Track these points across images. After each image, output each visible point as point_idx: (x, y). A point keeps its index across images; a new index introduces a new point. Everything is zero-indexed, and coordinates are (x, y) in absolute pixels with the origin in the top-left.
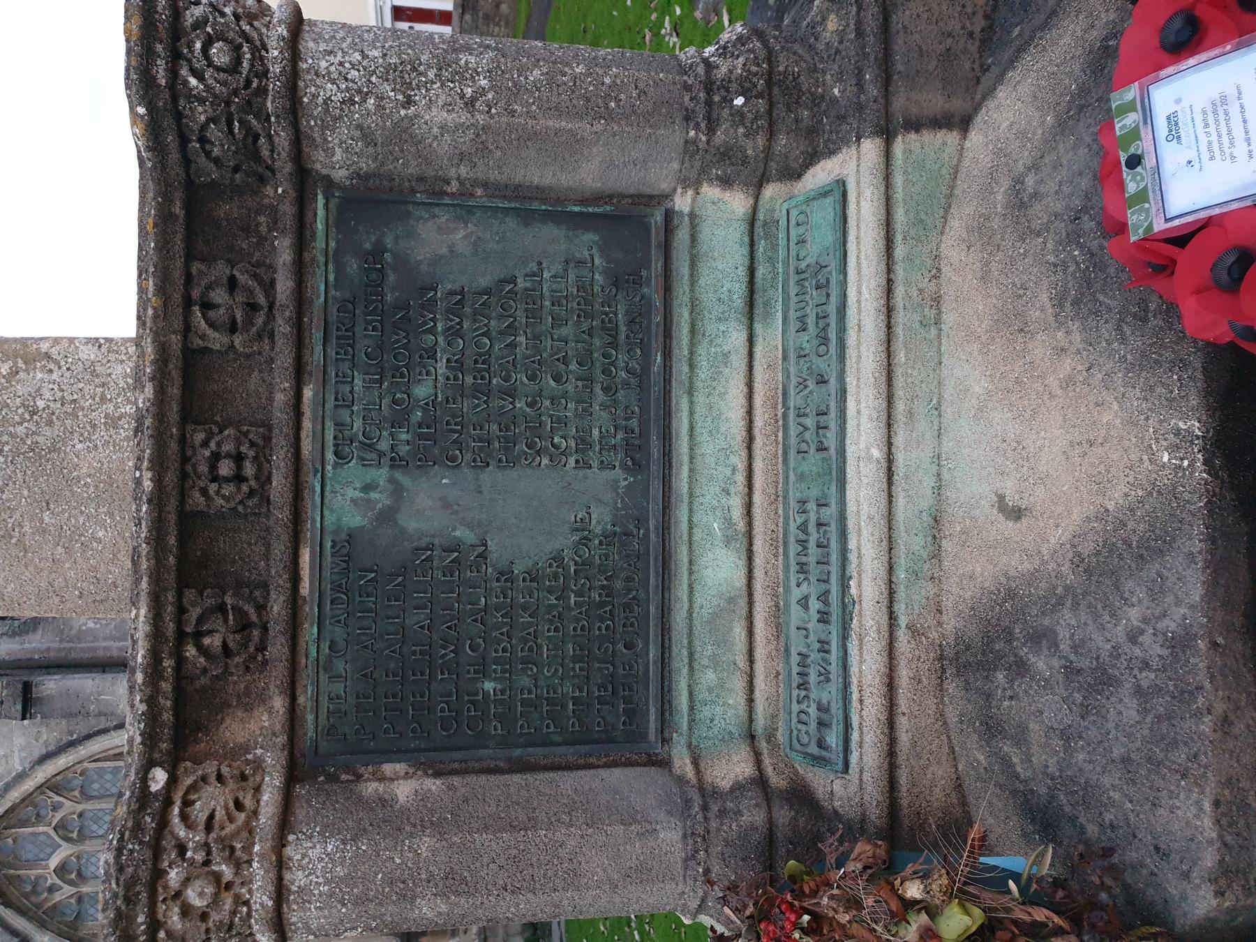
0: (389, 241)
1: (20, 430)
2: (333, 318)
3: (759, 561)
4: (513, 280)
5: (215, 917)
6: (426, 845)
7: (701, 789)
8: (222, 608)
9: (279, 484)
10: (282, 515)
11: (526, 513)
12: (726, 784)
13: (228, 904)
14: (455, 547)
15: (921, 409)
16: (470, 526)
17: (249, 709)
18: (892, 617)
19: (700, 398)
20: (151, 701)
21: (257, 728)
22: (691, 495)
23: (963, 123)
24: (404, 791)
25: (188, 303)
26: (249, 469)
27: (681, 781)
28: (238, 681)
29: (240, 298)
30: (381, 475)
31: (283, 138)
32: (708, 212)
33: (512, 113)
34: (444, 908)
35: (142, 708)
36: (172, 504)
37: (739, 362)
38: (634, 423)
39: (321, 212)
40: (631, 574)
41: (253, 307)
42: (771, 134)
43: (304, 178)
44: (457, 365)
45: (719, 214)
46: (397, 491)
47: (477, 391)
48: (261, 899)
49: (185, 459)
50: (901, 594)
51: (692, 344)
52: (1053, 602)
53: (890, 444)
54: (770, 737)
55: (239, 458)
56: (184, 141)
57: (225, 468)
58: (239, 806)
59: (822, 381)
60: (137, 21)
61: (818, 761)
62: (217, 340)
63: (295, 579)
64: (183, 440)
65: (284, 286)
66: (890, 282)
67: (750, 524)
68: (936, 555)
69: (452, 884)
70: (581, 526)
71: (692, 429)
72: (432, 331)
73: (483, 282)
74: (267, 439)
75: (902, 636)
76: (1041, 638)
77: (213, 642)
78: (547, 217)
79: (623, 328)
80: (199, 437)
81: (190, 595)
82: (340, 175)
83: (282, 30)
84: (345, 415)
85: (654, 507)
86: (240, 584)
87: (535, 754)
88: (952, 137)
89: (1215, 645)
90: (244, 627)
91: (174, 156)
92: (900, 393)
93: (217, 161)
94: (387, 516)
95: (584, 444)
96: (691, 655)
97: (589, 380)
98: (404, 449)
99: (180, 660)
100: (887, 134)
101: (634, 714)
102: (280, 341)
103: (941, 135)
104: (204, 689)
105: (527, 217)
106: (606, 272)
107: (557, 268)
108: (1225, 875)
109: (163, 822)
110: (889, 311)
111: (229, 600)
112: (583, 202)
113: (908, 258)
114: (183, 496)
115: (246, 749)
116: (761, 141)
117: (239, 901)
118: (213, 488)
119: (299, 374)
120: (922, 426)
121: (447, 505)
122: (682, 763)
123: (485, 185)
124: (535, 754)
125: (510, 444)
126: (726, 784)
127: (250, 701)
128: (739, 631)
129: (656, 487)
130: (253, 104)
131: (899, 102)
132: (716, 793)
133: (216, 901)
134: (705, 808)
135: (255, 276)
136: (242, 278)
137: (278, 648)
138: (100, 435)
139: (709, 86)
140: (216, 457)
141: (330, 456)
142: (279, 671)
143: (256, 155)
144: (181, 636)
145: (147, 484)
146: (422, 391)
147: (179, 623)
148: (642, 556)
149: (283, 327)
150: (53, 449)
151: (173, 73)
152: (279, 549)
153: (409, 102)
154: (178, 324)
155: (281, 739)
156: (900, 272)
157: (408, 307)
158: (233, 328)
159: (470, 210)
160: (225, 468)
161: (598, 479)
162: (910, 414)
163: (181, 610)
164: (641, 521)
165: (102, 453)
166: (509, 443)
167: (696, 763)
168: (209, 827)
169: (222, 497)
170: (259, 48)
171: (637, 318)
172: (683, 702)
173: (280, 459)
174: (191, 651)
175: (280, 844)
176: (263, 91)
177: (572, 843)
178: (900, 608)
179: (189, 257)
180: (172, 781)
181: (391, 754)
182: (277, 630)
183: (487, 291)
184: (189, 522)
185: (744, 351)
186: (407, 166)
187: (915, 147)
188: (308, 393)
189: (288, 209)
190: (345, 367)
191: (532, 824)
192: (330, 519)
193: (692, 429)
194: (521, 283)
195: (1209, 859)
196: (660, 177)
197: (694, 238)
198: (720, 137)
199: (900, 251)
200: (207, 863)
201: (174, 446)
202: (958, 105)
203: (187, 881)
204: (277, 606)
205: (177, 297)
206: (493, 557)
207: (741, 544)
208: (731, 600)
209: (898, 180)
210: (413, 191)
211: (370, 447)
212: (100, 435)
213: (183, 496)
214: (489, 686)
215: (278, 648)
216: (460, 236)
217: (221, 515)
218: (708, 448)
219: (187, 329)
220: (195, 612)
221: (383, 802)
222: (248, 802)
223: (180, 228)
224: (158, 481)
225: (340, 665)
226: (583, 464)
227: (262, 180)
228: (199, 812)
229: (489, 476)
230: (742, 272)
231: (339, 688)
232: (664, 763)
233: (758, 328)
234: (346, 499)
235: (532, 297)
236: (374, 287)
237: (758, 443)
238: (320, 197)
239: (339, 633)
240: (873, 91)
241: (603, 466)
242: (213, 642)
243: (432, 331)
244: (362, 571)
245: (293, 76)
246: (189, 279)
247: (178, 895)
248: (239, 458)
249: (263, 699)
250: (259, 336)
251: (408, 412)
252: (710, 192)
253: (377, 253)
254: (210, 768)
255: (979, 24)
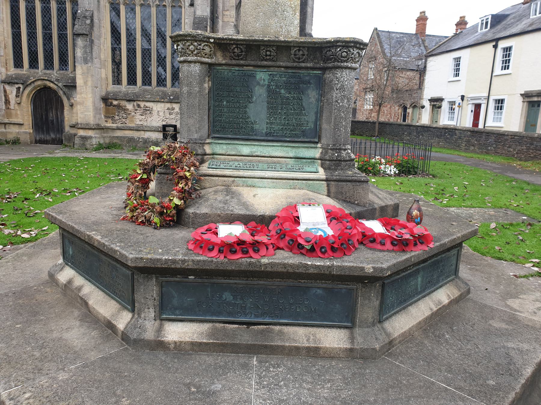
0: (312, 85)
1: (280, 9)
2: (297, 74)
3: (247, 158)
4: (304, 110)
5: (188, 50)
6: (197, 89)
7: (204, 143)
8: (242, 52)
9: (265, 63)
10: (259, 63)
11: (258, 112)
12: (205, 148)
13: (189, 53)
14: (252, 97)
15: (275, 184)
16: (256, 100)
17: (223, 56)
18: (236, 177)
19: (280, 148)
20: (226, 39)
21: (219, 58)
22: (261, 145)
23: (328, 196)
24: (206, 85)
25: (299, 47)
26: (268, 57)
27: (205, 140)
28: (228, 54)
29: (301, 57)
30: (266, 83)
31: (330, 65)
32: (317, 150)
33: (335, 110)
34: (185, 92)
35: (225, 37)
36: (261, 43)
37: (286, 155)
38: (275, 134)
39: (318, 72)
40: (247, 134)
41: (299, 59)
42: (329, 160)
43: (324, 69)
44: (288, 98)
45: (316, 153)
46: (263, 86)
47: (282, 102)
48: (190, 58)
49: (270, 46)
50: (240, 179)
51: (291, 147)
52: (239, 200)
53: (268, 179)
54: (213, 158)
55: (270, 55)
56: (329, 47)
57: (268, 53)
58: (206, 55)
59: (281, 168)
60: (348, 40)
61: (210, 164)
62: (293, 52)
63: (247, 66)
64: (273, 46)
65: (303, 65)
66: (298, 180)
67: (254, 156)
68: (247, 186)
69: (189, 93)
70: (255, 122)
71: (274, 146)
72: (294, 93)
73: (304, 104)
74: (274, 61)
75: (233, 179)
76: (232, 198)
77: (236, 50)
78: (316, 117)
79: (294, 132)
80: (274, 49)
81: (245, 46)
82: (325, 76)
83: (350, 66)
84: (278, 76)
85: (258, 138)
86: (246, 55)
87: (211, 111)
88: (326, 193)
89: (232, 214)
90: (238, 56)
91: (326, 45)
92: (277, 181)
93: (326, 53)
94: (258, 84)
95: (272, 123)
96: (229, 144)
97: (284, 125)
98: (271, 87)
99: (233, 44)
100: (327, 180)
101: (218, 132)
102: (292, 64)
103: (326, 191)
104: (227, 48)
105: (316, 113)
106: (305, 129)
107: (306, 119)
108: (195, 214)
109: (204, 42)
110: (293, 179)
111: (243, 53)
112: (320, 125)
113: (303, 183)
114: (263, 45)
115: (215, 56)
116: (328, 158)
117: (189, 55)
118: (265, 51)
119: (286, 67)
120: (271, 185)
121: (260, 95)
122: (208, 141)
123: (323, 105)
124: (211, 111)
125: (272, 108)
126: (205, 148)
127: (224, 57)
128: (233, 153)
129: (262, 138)
130: (336, 60)
131: (333, 183)
132: (203, 146)
133: (190, 50)
134: (201, 143)
135: (305, 59)
136: (304, 57)
137: (234, 62)
138: (278, 24)
139: (340, 149)
140: (270, 51)
141: (270, 73)
142: (230, 62)
143: (328, 60)
144: (237, 44)
145: (265, 39)
146: (283, 91)
147: (239, 44)
148: (249, 135)
149: (295, 64)
150: (276, 15)
151: (340, 46)
152: (253, 63)
153: (337, 89)
154: (295, 45)
155: (217, 62)
156: (300, 181)
157: (299, 89)
158: (295, 55)
159: (318, 102)
160: (268, 53)
161: (265, 126)
162: (274, 182)
163: (242, 45)
164: (256, 135)
165: (274, 25)
166: (272, 108)
167: (208, 143)
168: (203, 49)
169: (263, 52)
170: (345, 61)
171: (296, 136)
172: (216, 142)
173: (270, 63)
174: (234, 46)
175: (199, 62)
176: (338, 62)
177: (196, 117)
178: (238, 179)
179: (308, 47)
180: (211, 43)
181: (213, 83)
182: (238, 62)
183: (302, 105)
184: (258, 47)
185: (289, 156)
186: (326, 89)
187: (324, 186)
188: (283, 69)
189: (318, 66)
190: (287, 76)
191: (200, 109)
192: (258, 73)
193: (274, 146)
194: (303, 112)
195: (198, 212)
196: (324, 141)
197: (312, 147)
198: (330, 151)
199: (304, 182)
200: (197, 49)
201: (272, 44)
202: (332, 195)
203: (194, 46)
204: (242, 62)
205: (300, 45)
206: (249, 104)
207: (251, 154)
208: (240, 152)
209: (318, 182)
210: (322, 90)
211: (272, 80)
212: (278, 24)
213: (263, 45)
214: (225, 103)
215: (234, 62)
216: (313, 100)
217: (260, 52)
218: (270, 149)
219: (295, 47)
220: (241, 47)
221: (205, 81)
222: (206, 56)
223: (313, 46)
224: (266, 41)
225: (230, 74)
226: (267, 123)
227: (324, 61)
228: (206, 48)
229: (266, 104)
230: (304, 156)
231: (226, 73)
232: (208, 138)
233: (293, 159)
234: (262, 76)
235: (300, 114)
236: (304, 82)
237: (270, 159)
238: (320, 72)
239: (236, 74)
240: (335, 178)
241: (267, 128)
242: (236, 50)
243: (294, 93)
244: (247, 81)
245: (331, 68)
246: (304, 47)
247: (192, 44)
248: (270, 55)
249: (224, 59)
250: (294, 60)
251: (279, 88)
252: (320, 150)
253: (309, 83)
254: (213, 49)
255: (349, 200)
